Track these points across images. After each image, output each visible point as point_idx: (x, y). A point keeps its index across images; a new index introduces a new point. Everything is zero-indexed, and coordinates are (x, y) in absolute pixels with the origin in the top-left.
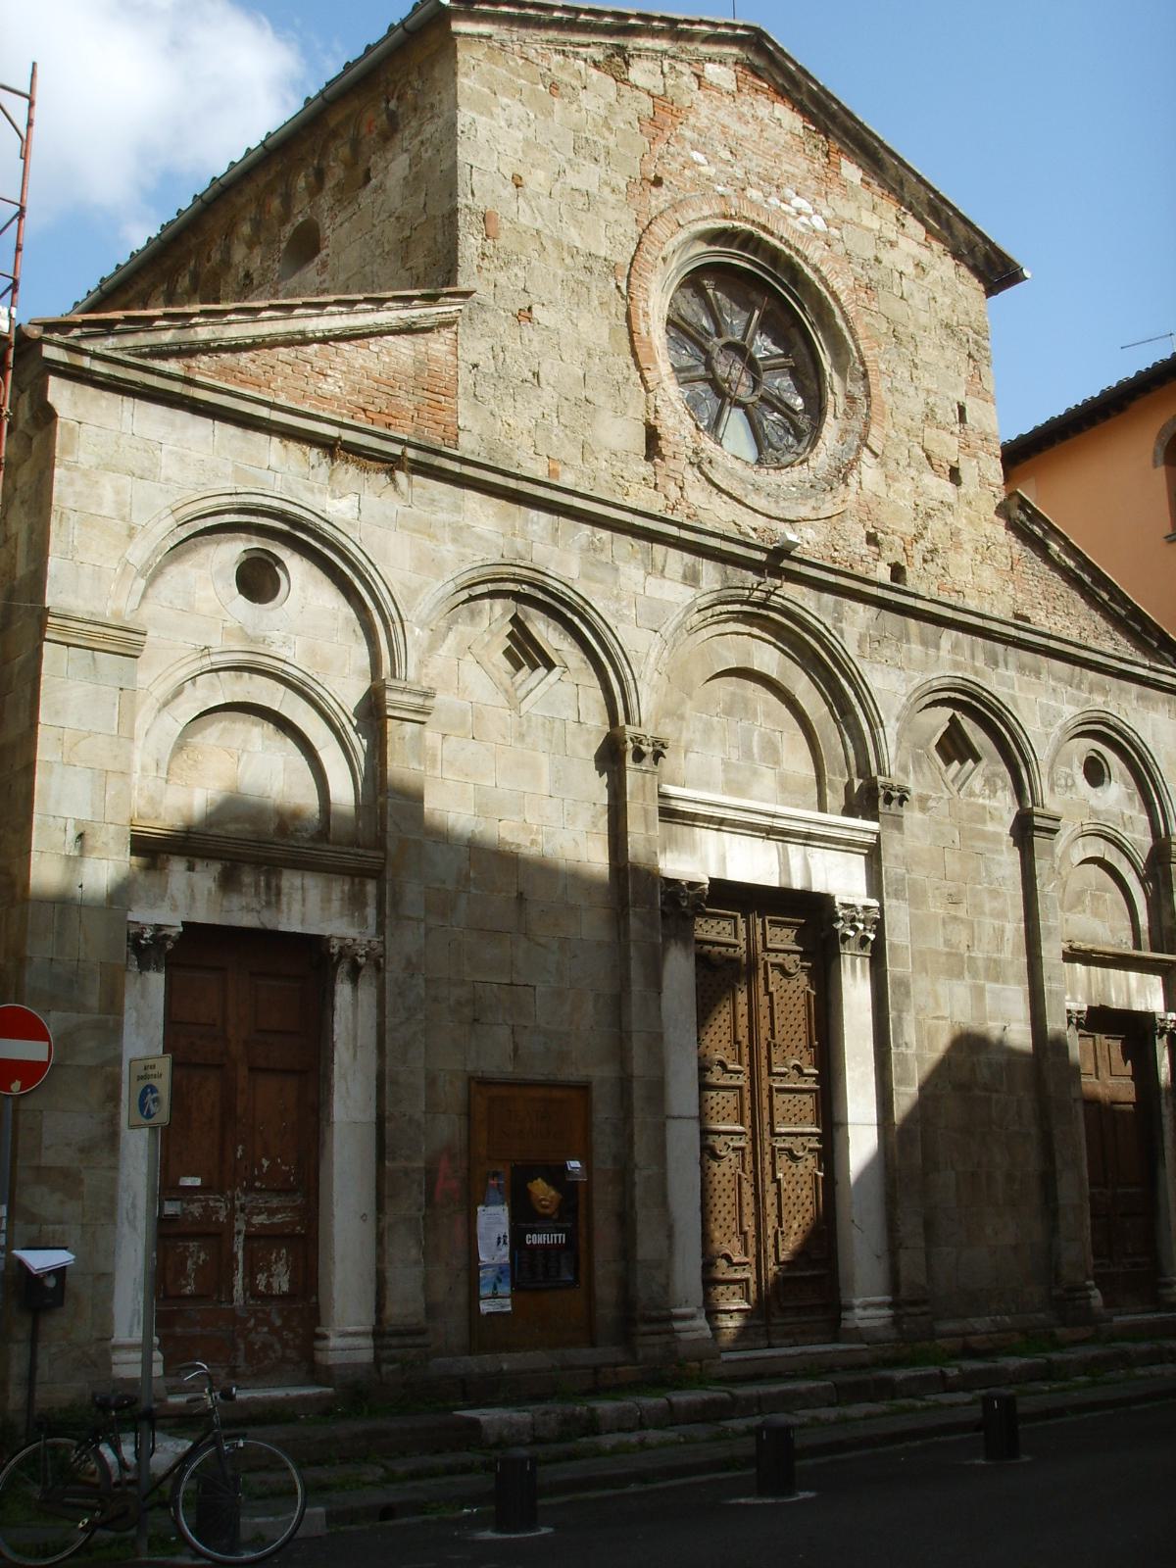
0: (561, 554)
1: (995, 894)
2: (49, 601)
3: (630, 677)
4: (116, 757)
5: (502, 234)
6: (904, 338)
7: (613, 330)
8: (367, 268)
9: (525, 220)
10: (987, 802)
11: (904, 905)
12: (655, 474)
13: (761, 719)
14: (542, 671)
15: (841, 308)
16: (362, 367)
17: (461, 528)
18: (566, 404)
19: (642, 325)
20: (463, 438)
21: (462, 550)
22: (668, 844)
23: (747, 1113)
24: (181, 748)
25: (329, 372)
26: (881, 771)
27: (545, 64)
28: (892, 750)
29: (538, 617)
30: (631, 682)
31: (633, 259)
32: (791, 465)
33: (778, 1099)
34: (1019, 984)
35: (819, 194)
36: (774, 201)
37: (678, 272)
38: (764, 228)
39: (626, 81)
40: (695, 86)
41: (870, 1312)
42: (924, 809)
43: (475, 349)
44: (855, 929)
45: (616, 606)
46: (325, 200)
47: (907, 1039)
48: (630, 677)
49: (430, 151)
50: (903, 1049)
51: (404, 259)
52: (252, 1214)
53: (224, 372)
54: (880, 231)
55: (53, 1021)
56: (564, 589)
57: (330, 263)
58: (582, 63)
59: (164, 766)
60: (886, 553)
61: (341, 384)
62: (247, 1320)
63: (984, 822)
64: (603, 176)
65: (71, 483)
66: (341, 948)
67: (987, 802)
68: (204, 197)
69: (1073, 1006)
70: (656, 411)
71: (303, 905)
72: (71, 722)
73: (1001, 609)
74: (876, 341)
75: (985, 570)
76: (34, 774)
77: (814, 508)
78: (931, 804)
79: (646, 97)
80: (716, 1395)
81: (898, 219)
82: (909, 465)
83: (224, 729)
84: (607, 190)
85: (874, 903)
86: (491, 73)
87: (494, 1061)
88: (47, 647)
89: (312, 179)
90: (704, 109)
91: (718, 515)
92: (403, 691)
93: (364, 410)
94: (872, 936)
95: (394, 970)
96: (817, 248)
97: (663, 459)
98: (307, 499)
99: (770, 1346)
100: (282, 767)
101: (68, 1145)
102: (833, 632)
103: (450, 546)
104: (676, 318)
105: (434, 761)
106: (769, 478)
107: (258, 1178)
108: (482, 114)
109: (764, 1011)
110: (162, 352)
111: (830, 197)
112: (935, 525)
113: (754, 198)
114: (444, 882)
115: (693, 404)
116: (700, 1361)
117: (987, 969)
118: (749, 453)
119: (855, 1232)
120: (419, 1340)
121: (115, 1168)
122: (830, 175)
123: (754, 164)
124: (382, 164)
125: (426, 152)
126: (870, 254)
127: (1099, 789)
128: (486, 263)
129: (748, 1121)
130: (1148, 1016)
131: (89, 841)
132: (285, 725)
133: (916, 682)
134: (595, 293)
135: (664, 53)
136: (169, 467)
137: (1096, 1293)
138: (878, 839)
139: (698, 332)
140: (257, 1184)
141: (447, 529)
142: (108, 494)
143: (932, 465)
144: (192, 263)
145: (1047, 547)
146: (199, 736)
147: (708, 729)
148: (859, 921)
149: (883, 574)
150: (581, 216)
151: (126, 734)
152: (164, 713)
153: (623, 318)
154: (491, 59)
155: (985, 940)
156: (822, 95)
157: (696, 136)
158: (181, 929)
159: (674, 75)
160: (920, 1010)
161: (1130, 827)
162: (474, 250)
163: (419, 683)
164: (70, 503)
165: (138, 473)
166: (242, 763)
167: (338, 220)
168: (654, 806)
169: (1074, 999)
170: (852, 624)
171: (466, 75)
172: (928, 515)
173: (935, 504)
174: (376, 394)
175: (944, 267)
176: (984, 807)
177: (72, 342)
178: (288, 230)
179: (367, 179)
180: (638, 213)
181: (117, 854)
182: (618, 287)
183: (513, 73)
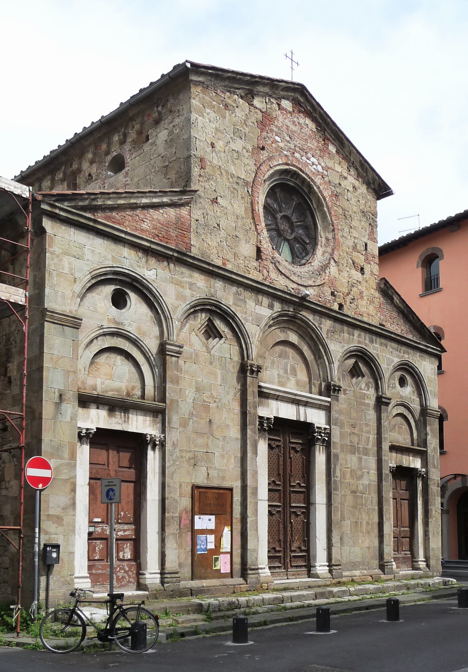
0: (226, 296)
1: (367, 425)
2: (47, 305)
3: (249, 343)
4: (72, 366)
5: (207, 167)
6: (348, 216)
7: (246, 209)
8: (148, 177)
9: (215, 162)
10: (366, 392)
11: (338, 428)
12: (259, 266)
13: (291, 359)
14: (217, 339)
15: (326, 203)
16: (157, 219)
17: (192, 284)
18: (229, 237)
19: (257, 207)
20: (193, 249)
21: (193, 292)
22: (260, 404)
23: (282, 499)
24: (92, 363)
25: (145, 220)
26: (332, 379)
27: (223, 96)
28: (336, 372)
29: (216, 319)
30: (250, 344)
31: (254, 180)
32: (304, 264)
33: (292, 495)
34: (374, 457)
35: (320, 156)
36: (304, 158)
37: (268, 186)
38: (301, 170)
39: (252, 105)
40: (277, 109)
41: (322, 568)
42: (345, 394)
43: (197, 213)
44: (321, 436)
45: (245, 316)
46: (127, 147)
47: (337, 475)
48: (249, 343)
49: (178, 130)
50: (336, 478)
51: (166, 174)
52: (118, 531)
53: (106, 218)
54: (341, 173)
55: (52, 463)
56: (227, 309)
57: (130, 173)
58: (236, 96)
59: (87, 369)
60: (337, 299)
61: (149, 225)
62: (117, 568)
63: (365, 399)
64: (244, 145)
65: (53, 259)
66: (150, 438)
67: (366, 392)
68: (71, 141)
69: (391, 465)
70: (260, 242)
71: (137, 422)
72: (56, 352)
73: (375, 322)
74: (338, 217)
75: (370, 308)
76: (43, 371)
77: (314, 282)
78: (347, 392)
79: (259, 112)
80: (277, 595)
81: (348, 168)
82: (347, 266)
83: (107, 357)
84: (245, 151)
85: (328, 427)
86: (203, 98)
87: (201, 480)
88: (46, 323)
89: (121, 137)
90: (281, 119)
91: (281, 283)
92: (172, 345)
93: (158, 236)
94: (327, 439)
95: (168, 447)
96: (319, 179)
97: (262, 260)
98: (138, 270)
99: (288, 579)
100: (128, 371)
101: (59, 507)
102: (318, 328)
103: (188, 291)
104: (267, 206)
105: (181, 371)
106: (297, 269)
107: (120, 519)
108: (200, 116)
109: (288, 464)
110: (84, 209)
111: (324, 158)
112: (354, 289)
113: (297, 157)
114: (184, 415)
115: (272, 239)
116: (267, 584)
117: (363, 451)
118: (290, 259)
119: (317, 541)
120: (177, 575)
121: (74, 515)
122: (325, 149)
123: (298, 143)
124: (154, 134)
125: (176, 130)
126: (337, 182)
127: (403, 388)
128: (201, 179)
129: (282, 502)
130: (415, 470)
131: (63, 397)
132: (128, 356)
133: (345, 348)
134: (240, 193)
135: (267, 94)
136: (88, 255)
137: (394, 563)
138: (330, 405)
139: (273, 210)
140: (120, 521)
141: (188, 284)
142: (67, 266)
143: (355, 267)
144: (63, 168)
145: (393, 299)
146: (99, 359)
147: (273, 363)
148: (323, 433)
149: (336, 307)
150: (235, 160)
151: (76, 357)
152: (87, 350)
153: (249, 204)
154: (203, 93)
155: (363, 441)
156: (325, 115)
157: (277, 130)
158: (95, 430)
159: (270, 104)
160: (341, 465)
161: (413, 403)
162: (196, 173)
163: (177, 342)
164: (53, 268)
165: (77, 257)
166: (114, 370)
167: (133, 156)
168: (256, 390)
169: (391, 463)
170: (325, 326)
171: (194, 99)
172: (353, 286)
173: (355, 282)
174: (162, 230)
175: (363, 188)
176: (365, 394)
177: (52, 202)
178: (109, 158)
179: (148, 139)
180: (256, 161)
181: (73, 402)
182: (248, 191)
183: (211, 99)
